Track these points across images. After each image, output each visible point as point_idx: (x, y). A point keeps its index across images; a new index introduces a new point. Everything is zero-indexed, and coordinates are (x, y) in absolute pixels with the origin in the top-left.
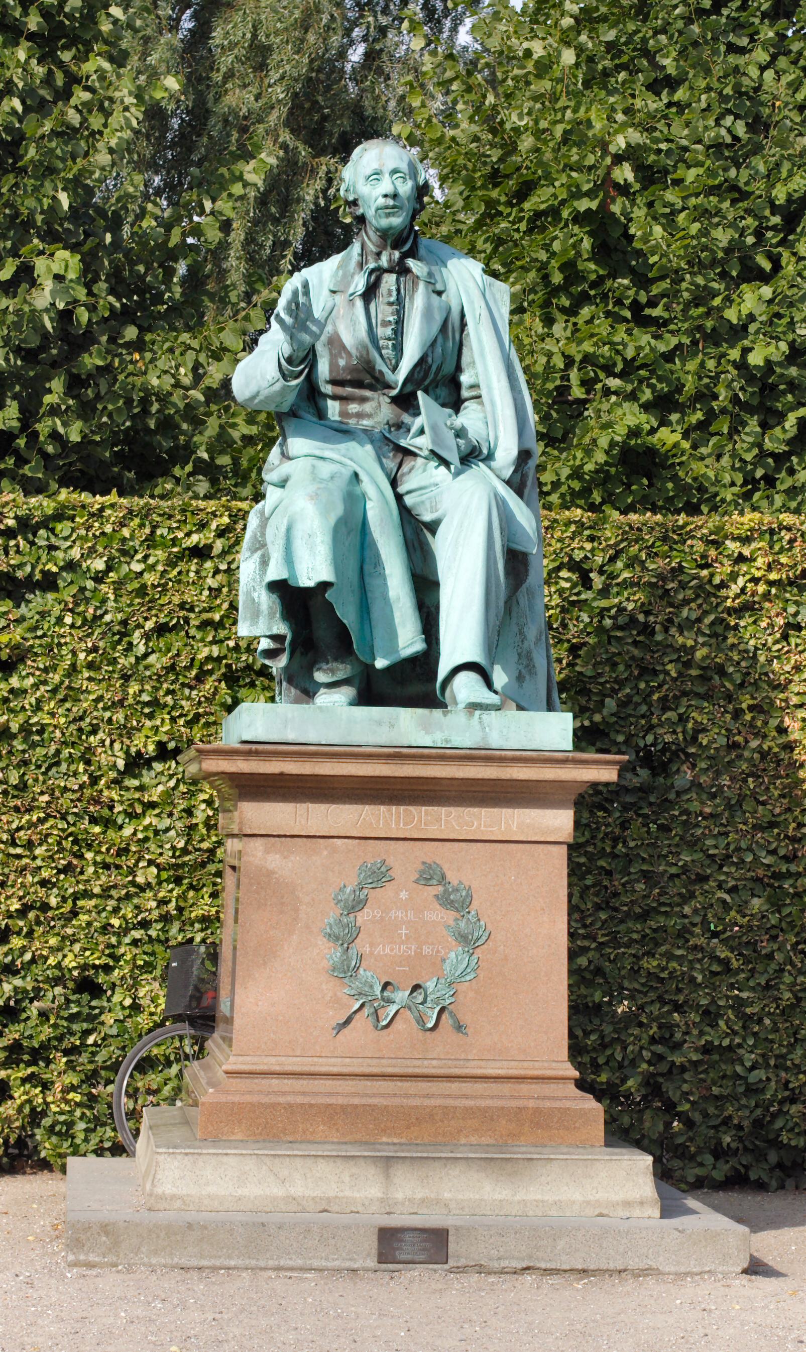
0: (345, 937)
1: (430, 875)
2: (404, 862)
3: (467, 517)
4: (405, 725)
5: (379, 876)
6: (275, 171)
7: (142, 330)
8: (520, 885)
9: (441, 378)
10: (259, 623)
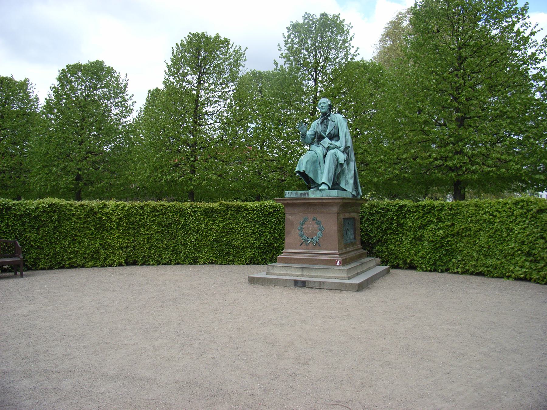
1: (314, 219)
2: (310, 216)
5: (306, 220)
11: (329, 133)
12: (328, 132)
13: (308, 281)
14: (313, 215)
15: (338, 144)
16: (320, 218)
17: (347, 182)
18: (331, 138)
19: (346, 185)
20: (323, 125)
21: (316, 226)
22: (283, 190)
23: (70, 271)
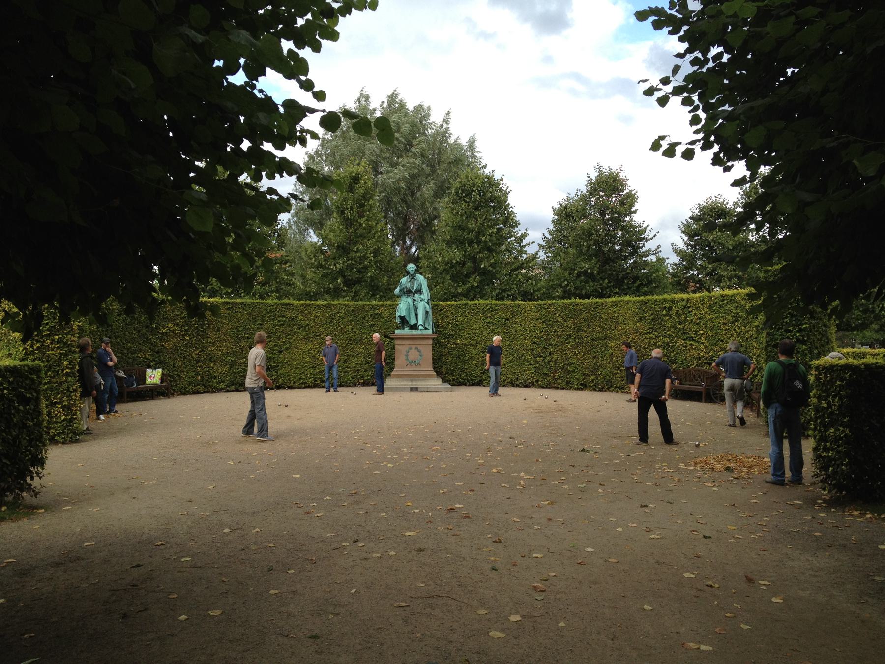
0: (407, 356)
1: (416, 348)
3: (422, 307)
4: (414, 332)
5: (411, 349)
6: (144, 537)
7: (417, 271)
8: (427, 352)
9: (419, 291)
10: (398, 320)
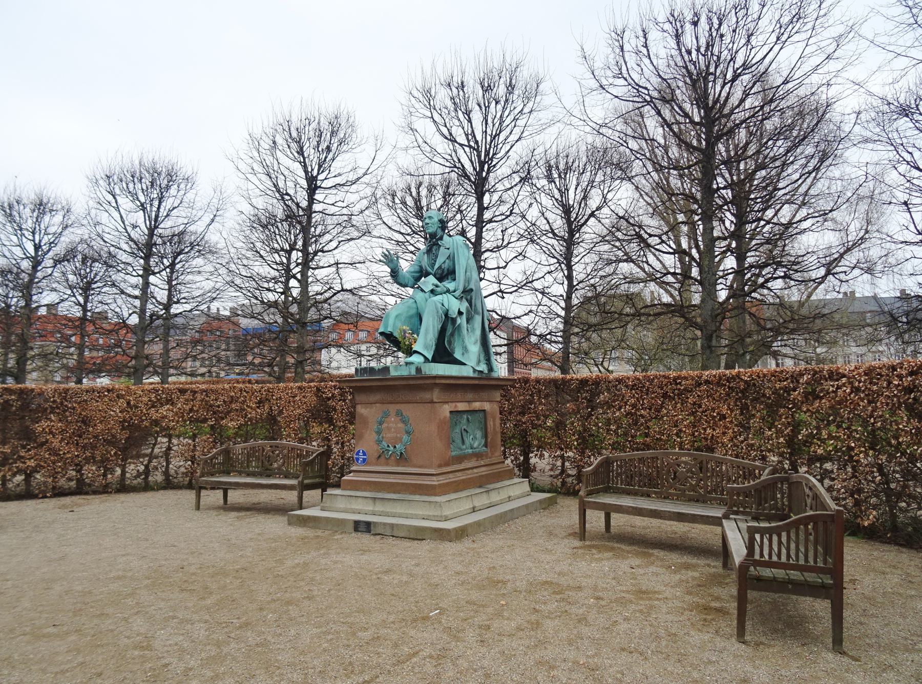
1: (399, 413)
2: (392, 408)
5: (386, 415)
11: (440, 267)
12: (436, 266)
13: (375, 523)
14: (398, 406)
15: (451, 286)
16: (409, 410)
17: (465, 350)
18: (441, 279)
19: (463, 354)
20: (431, 255)
21: (400, 425)
22: (169, 329)
23: (122, 497)
